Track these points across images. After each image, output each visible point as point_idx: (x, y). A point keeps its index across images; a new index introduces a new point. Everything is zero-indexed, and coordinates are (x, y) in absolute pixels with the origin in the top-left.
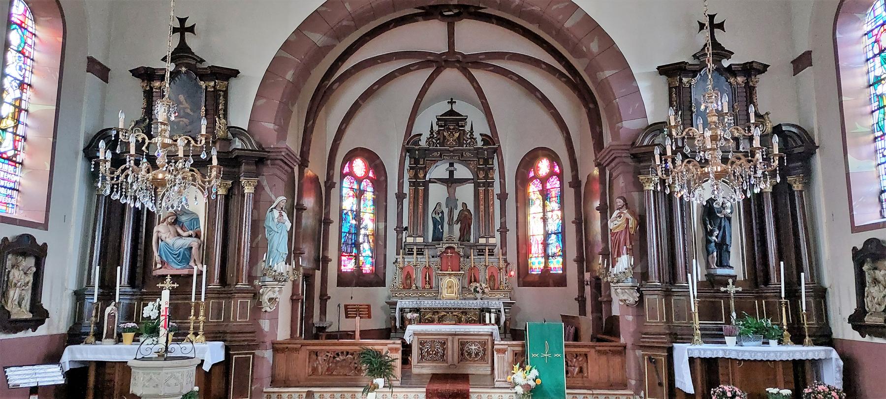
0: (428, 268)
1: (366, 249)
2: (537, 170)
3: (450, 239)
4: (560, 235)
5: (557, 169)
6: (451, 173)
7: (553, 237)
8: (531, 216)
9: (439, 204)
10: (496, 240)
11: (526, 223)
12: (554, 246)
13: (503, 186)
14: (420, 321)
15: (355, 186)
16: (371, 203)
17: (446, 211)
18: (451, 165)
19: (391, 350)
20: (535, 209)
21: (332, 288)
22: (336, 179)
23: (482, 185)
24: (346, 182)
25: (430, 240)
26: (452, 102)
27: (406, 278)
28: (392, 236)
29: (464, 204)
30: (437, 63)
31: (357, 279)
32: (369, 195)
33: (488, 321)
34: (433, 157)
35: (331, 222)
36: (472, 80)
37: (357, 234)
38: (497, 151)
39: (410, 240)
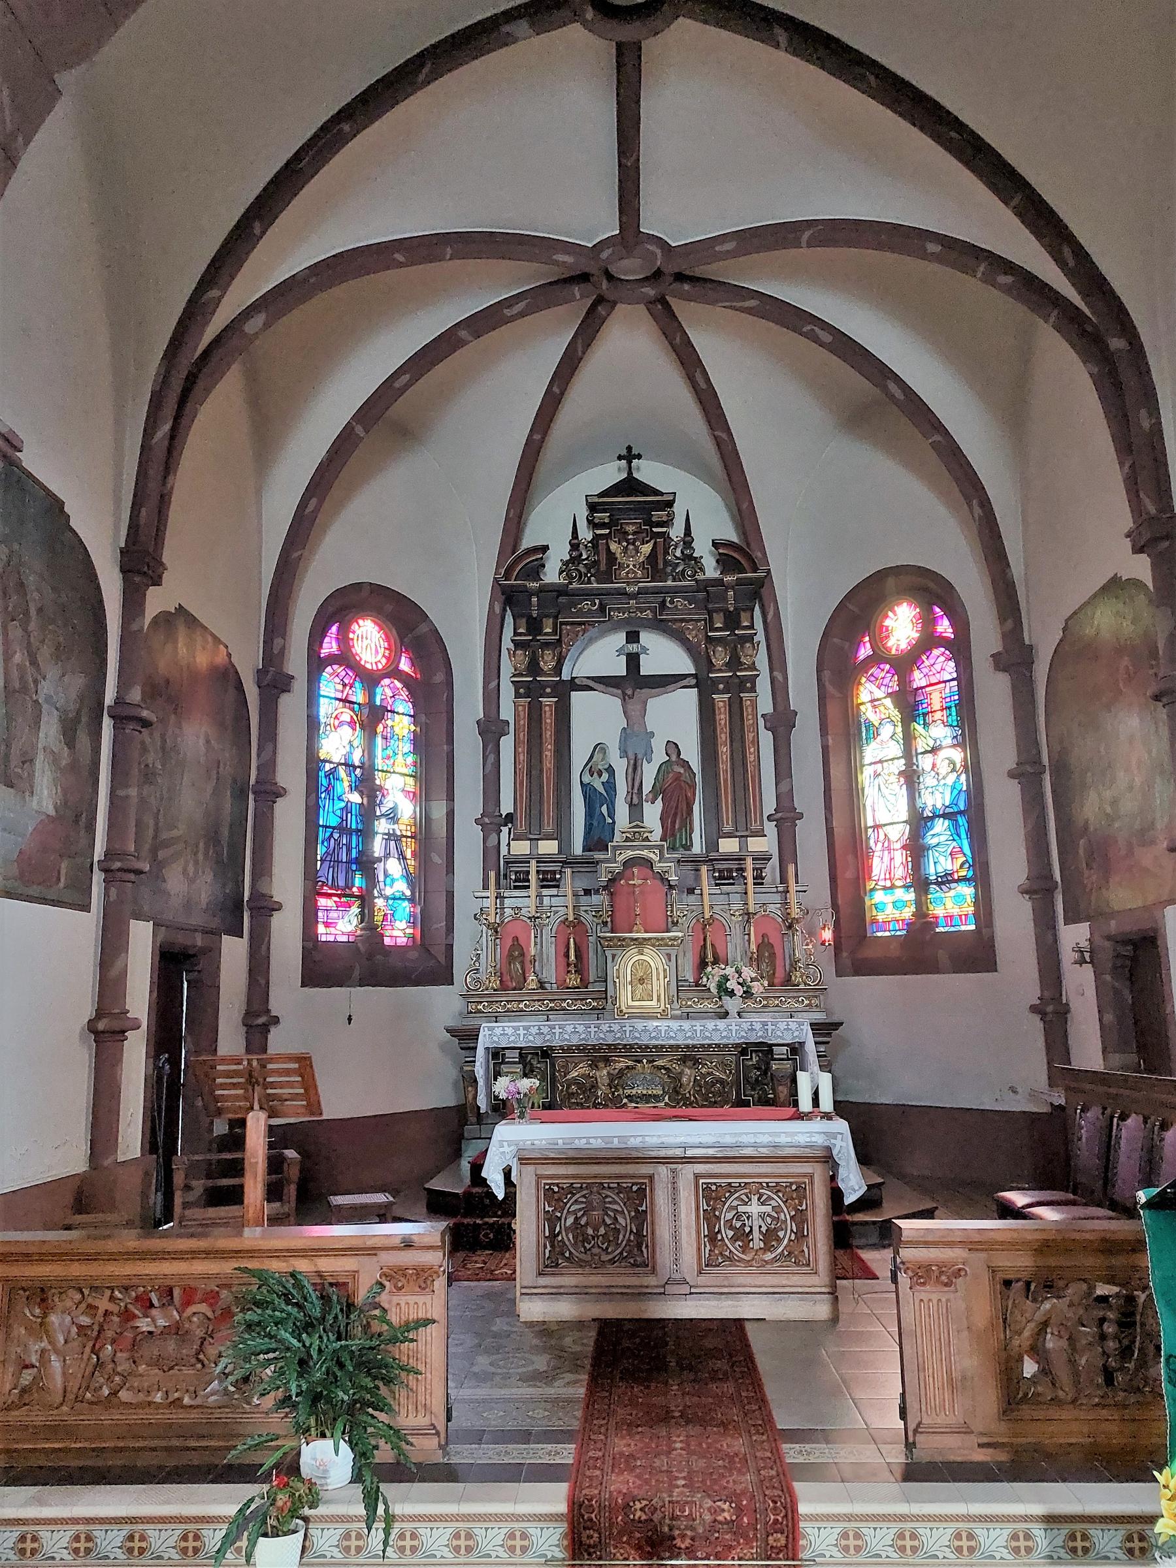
0: (575, 925)
1: (394, 877)
2: (878, 643)
3: (637, 834)
4: (962, 821)
5: (945, 627)
6: (633, 661)
7: (941, 825)
8: (868, 771)
9: (599, 748)
10: (765, 844)
11: (854, 794)
12: (946, 851)
13: (779, 690)
14: (556, 1101)
15: (359, 696)
16: (408, 747)
17: (621, 767)
18: (633, 637)
19: (396, 1277)
20: (881, 752)
21: (286, 989)
22: (296, 663)
23: (720, 688)
24: (330, 685)
25: (578, 849)
26: (630, 456)
27: (511, 959)
28: (469, 843)
29: (673, 747)
30: (588, 285)
31: (368, 965)
32: (402, 724)
33: (805, 1104)
34: (580, 613)
35: (279, 793)
36: (689, 361)
37: (366, 833)
38: (758, 590)
39: (521, 848)
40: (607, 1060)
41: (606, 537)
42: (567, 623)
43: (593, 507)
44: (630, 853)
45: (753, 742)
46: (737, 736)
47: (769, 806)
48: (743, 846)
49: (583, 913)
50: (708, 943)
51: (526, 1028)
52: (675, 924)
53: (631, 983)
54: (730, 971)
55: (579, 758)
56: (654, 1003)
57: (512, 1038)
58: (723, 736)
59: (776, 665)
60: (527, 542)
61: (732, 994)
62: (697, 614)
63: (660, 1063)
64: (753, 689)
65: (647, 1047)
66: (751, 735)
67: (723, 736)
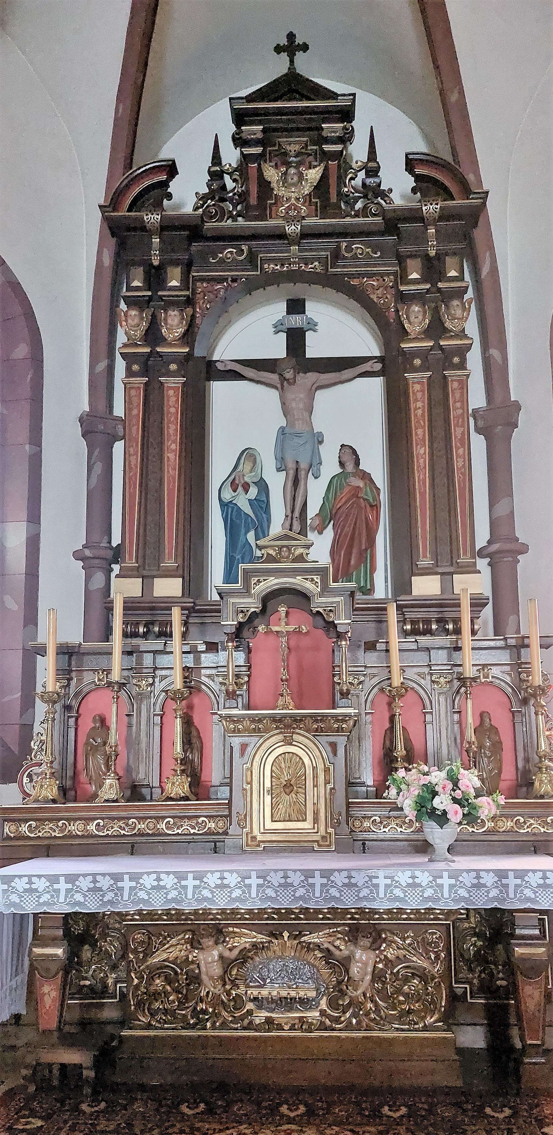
6: (296, 339)
9: (248, 455)
17: (277, 483)
18: (296, 306)
23: (412, 374)
29: (349, 455)
40: (219, 933)
41: (261, 157)
42: (202, 279)
43: (240, 118)
44: (273, 582)
45: (462, 441)
46: (440, 433)
47: (482, 536)
48: (447, 585)
49: (204, 679)
50: (398, 727)
51: (71, 878)
52: (345, 695)
53: (271, 791)
54: (438, 777)
55: (219, 467)
56: (307, 825)
57: (45, 898)
58: (420, 432)
59: (492, 338)
60: (143, 160)
61: (442, 819)
62: (384, 265)
63: (314, 938)
64: (462, 365)
65: (289, 911)
66: (459, 431)
67: (420, 432)
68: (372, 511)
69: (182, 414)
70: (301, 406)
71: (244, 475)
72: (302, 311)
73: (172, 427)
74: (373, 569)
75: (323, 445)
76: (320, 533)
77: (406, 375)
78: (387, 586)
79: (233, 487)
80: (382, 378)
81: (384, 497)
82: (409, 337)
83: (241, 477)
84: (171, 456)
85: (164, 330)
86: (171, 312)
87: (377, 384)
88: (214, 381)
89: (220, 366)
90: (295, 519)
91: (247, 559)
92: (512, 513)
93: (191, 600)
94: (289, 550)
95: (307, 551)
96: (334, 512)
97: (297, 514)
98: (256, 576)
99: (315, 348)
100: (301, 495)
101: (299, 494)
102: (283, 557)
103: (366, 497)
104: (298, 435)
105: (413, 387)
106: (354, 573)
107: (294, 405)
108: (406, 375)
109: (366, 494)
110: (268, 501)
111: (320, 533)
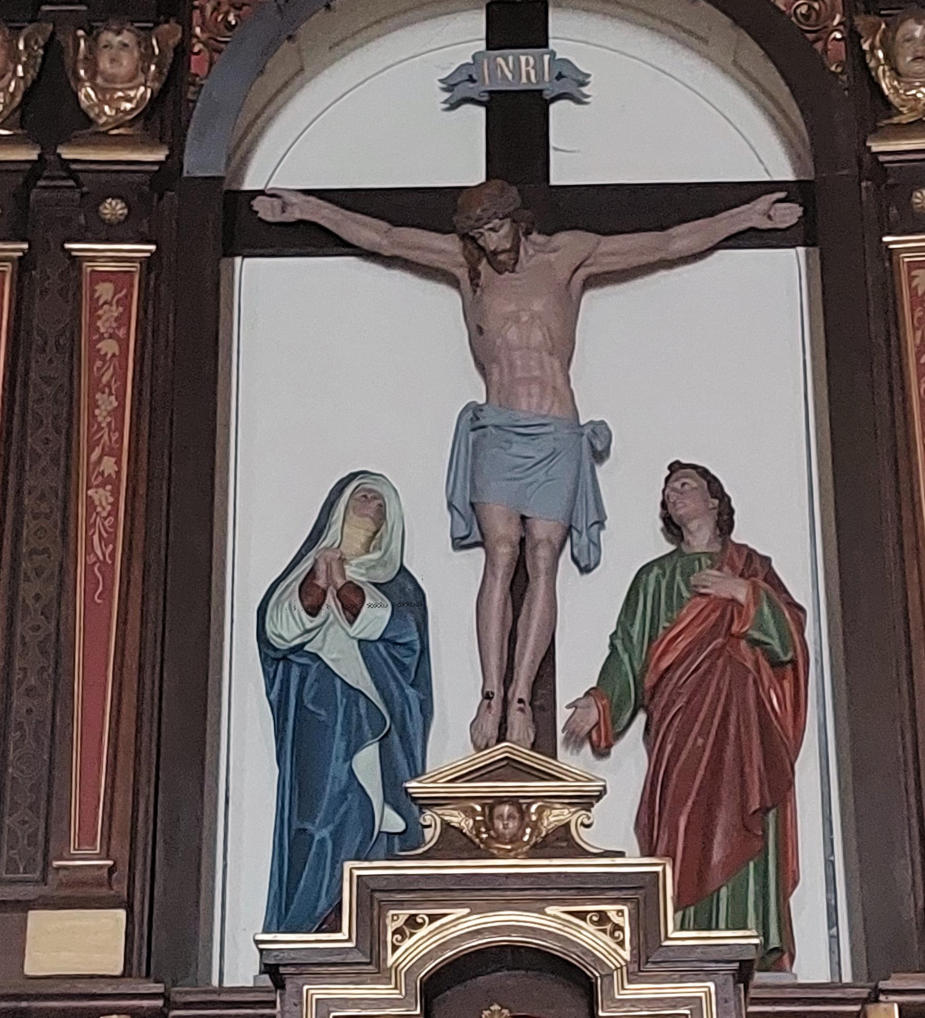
6: (517, 126)
9: (360, 496)
17: (454, 586)
29: (697, 497)
44: (462, 926)
55: (262, 530)
68: (781, 679)
69: (139, 360)
70: (537, 336)
71: (342, 561)
72: (538, 38)
73: (106, 403)
74: (788, 879)
75: (607, 464)
76: (601, 752)
77: (886, 239)
78: (834, 939)
79: (309, 601)
80: (801, 250)
81: (817, 635)
82: (896, 120)
83: (335, 566)
84: (102, 496)
85: (87, 94)
86: (108, 37)
87: (788, 266)
88: (244, 257)
89: (265, 210)
90: (515, 705)
91: (353, 839)
92: (587, 694)
93: (159, 988)
94: (523, 813)
95: (582, 816)
96: (649, 680)
97: (521, 689)
98: (401, 904)
99: (579, 153)
100: (534, 624)
101: (528, 627)
102: (499, 838)
103: (757, 635)
104: (527, 432)
105: (911, 278)
106: (724, 892)
107: (512, 334)
108: (886, 239)
109: (761, 628)
110: (425, 650)
111: (601, 752)
